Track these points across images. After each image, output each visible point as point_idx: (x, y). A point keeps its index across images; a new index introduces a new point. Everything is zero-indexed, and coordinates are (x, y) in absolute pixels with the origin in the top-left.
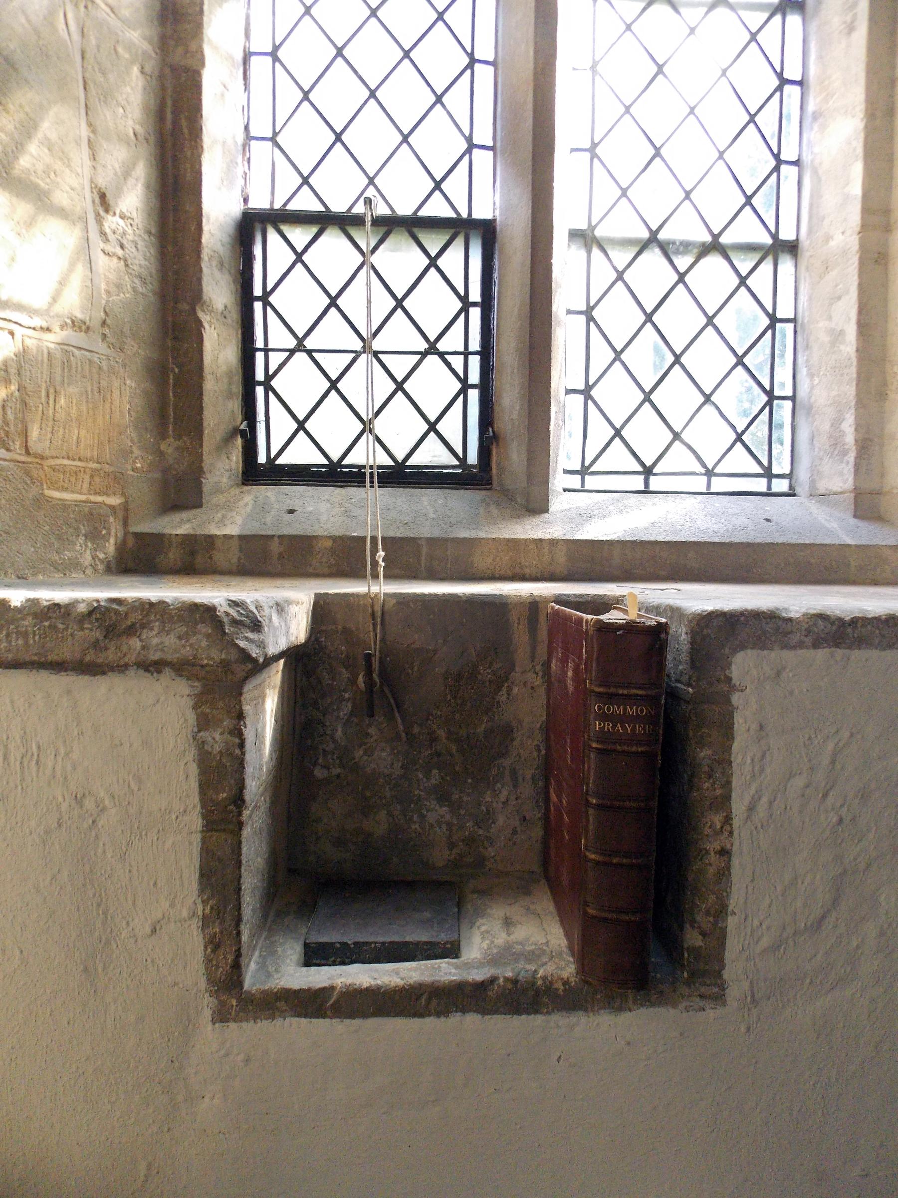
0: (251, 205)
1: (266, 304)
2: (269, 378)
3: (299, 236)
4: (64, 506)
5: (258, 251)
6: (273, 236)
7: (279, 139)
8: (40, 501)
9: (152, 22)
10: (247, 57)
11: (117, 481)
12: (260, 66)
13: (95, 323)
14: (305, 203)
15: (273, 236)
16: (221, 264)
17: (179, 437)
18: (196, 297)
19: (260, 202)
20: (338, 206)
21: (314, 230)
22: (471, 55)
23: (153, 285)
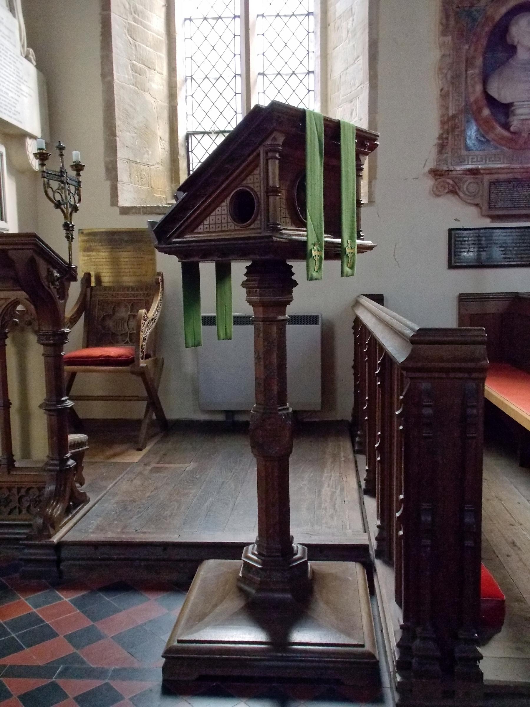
0: (188, 131)
1: (192, 152)
2: (192, 150)
3: (199, 137)
4: (157, 197)
5: (190, 141)
6: (193, 137)
7: (194, 115)
8: (154, 196)
9: (316, 601)
10: (186, 97)
11: (164, 192)
12: (189, 98)
13: (160, 162)
14: (200, 129)
15: (193, 137)
16: (182, 145)
17: (175, 183)
18: (178, 154)
19: (190, 130)
20: (207, 130)
21: (202, 135)
22: (235, 93)
23: (169, 153)
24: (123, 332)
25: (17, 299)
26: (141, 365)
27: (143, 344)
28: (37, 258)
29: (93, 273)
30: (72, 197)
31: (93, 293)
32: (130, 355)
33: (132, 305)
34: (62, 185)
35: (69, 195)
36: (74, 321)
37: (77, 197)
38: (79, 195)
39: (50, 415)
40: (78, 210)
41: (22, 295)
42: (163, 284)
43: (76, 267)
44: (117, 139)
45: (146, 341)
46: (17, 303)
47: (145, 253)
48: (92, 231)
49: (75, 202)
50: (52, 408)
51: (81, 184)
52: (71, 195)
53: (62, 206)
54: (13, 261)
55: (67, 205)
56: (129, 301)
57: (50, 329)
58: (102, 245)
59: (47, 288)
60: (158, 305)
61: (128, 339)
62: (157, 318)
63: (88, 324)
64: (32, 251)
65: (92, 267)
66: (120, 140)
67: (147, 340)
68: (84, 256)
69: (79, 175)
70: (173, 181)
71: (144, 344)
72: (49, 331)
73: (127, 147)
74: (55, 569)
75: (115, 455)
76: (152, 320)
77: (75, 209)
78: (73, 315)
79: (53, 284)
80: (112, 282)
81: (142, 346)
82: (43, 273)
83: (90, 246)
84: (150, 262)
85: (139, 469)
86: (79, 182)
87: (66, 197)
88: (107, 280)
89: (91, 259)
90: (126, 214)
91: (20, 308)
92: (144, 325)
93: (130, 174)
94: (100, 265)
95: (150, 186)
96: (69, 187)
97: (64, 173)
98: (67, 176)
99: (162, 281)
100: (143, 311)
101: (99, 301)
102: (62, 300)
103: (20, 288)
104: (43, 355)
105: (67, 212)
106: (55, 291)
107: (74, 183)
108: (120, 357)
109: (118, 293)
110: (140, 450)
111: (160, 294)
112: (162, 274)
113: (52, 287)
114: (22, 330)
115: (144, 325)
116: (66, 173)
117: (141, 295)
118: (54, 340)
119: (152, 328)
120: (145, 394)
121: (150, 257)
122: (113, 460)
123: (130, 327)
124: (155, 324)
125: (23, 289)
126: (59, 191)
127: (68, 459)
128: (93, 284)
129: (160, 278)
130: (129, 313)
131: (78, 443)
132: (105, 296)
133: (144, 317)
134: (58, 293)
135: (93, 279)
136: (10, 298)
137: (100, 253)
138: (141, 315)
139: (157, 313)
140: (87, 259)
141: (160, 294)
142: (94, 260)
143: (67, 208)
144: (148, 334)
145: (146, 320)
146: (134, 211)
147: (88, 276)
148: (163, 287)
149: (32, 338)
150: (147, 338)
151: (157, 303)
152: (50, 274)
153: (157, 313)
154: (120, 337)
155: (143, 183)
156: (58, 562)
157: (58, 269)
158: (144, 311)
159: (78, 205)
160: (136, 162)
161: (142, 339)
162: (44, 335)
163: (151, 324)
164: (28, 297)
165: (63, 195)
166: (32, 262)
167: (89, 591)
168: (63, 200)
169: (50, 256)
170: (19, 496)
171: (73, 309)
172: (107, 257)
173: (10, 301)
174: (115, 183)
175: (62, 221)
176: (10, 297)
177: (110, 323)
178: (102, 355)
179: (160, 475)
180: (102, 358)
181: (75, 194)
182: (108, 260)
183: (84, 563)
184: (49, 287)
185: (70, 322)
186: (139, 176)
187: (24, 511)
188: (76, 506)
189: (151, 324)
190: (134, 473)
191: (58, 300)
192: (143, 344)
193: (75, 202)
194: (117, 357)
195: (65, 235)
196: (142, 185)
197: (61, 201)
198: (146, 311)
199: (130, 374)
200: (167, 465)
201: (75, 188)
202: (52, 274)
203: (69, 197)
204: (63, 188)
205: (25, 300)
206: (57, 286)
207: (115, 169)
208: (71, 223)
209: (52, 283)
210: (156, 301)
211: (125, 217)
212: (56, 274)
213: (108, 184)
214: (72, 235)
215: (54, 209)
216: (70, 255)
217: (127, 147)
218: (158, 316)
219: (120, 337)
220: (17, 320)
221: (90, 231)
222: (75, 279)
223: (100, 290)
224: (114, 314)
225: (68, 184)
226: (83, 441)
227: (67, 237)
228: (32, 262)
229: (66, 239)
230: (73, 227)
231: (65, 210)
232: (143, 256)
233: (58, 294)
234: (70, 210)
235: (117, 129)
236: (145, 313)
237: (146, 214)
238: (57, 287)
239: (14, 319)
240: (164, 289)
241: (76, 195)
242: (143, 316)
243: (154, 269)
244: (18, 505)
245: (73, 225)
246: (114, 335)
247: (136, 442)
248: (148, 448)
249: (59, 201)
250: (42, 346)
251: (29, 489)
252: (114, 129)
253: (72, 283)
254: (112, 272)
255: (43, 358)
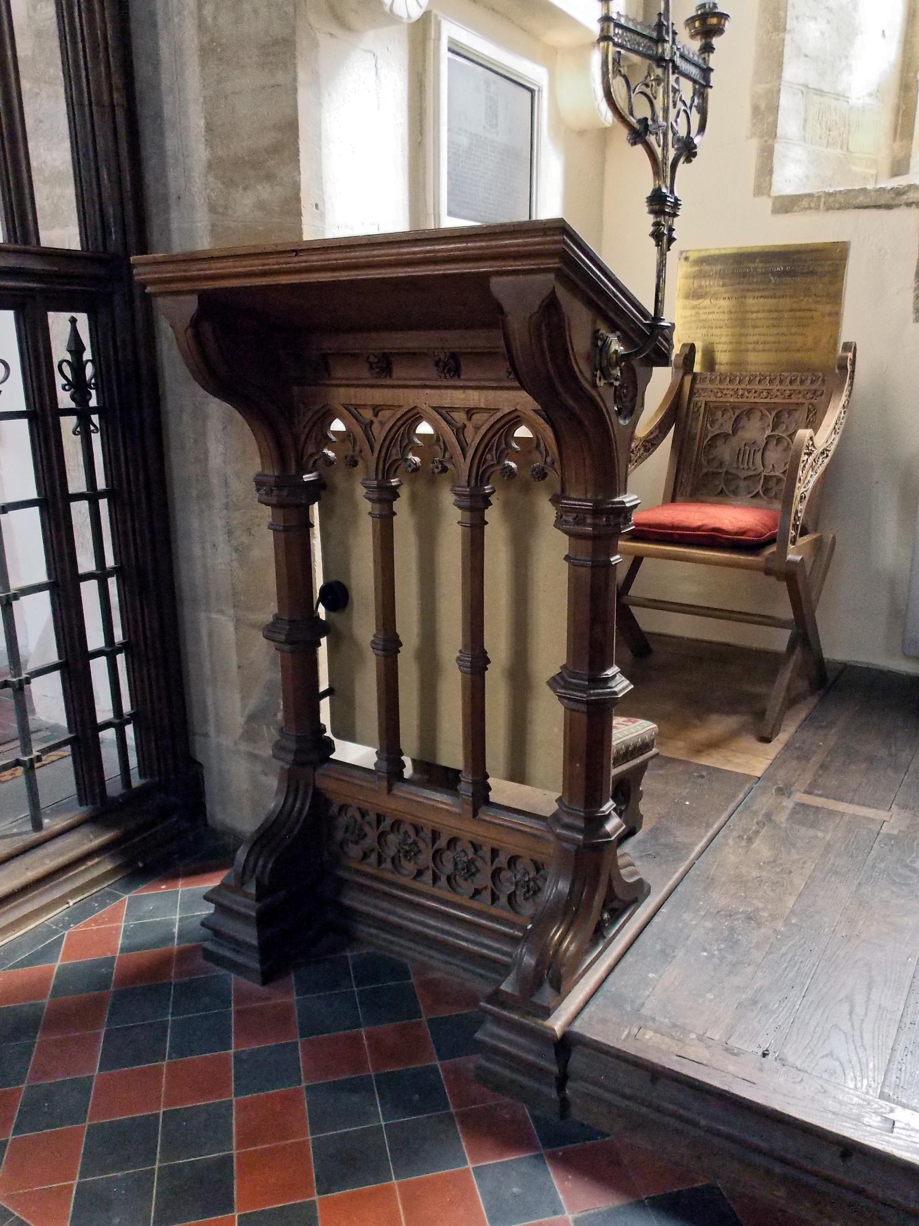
17: (901, 140)
24: (752, 473)
25: (516, 410)
26: (790, 557)
27: (800, 507)
28: (563, 295)
29: (699, 346)
30: (682, 114)
31: (697, 386)
32: (763, 530)
33: (778, 416)
34: (659, 71)
35: (675, 105)
36: (653, 445)
37: (695, 117)
38: (703, 112)
39: (572, 710)
40: (695, 155)
41: (523, 400)
42: (853, 371)
43: (673, 325)
44: (788, 37)
45: (805, 502)
46: (515, 420)
47: (819, 299)
48: (708, 253)
49: (689, 132)
50: (579, 695)
51: (713, 76)
52: (680, 105)
53: (652, 139)
54: (500, 309)
55: (665, 135)
56: (770, 407)
57: (589, 496)
58: (724, 285)
59: (587, 386)
60: (839, 418)
61: (759, 488)
62: (833, 448)
63: (679, 448)
64: (552, 276)
65: (699, 331)
66: (792, 40)
67: (807, 498)
68: (685, 308)
69: (708, 48)
70: (898, 136)
71: (800, 507)
72: (585, 501)
73: (806, 56)
74: (554, 1095)
75: (714, 745)
76: (823, 453)
77: (688, 150)
78: (651, 433)
79: (606, 375)
80: (727, 364)
81: (797, 512)
82: (580, 343)
83: (700, 287)
84: (827, 319)
85: (765, 801)
86: (707, 71)
87: (666, 111)
88: (722, 357)
89: (698, 313)
90: (786, 212)
91: (522, 432)
92: (804, 466)
93: (805, 120)
94: (716, 328)
95: (845, 148)
96: (677, 80)
97: (667, 33)
98: (674, 42)
99: (853, 363)
100: (804, 433)
101: (706, 404)
102: (625, 418)
103: (517, 384)
104: (567, 558)
105: (665, 157)
106: (609, 395)
107: (694, 72)
108: (743, 533)
109: (748, 387)
110: (766, 740)
111: (845, 393)
112: (855, 348)
113: (601, 383)
114: (526, 489)
115: (804, 466)
116: (675, 33)
117: (800, 393)
118: (594, 525)
119: (821, 470)
120: (786, 612)
121: (828, 308)
122: (705, 761)
123: (766, 463)
124: (827, 461)
125: (523, 387)
126: (648, 91)
127: (607, 818)
128: (697, 368)
129: (850, 355)
130: (768, 432)
131: (635, 747)
132: (720, 394)
133: (807, 447)
134: (617, 398)
135: (698, 357)
136: (498, 410)
137: (717, 302)
138: (802, 442)
139: (833, 436)
140: (691, 316)
141: (845, 393)
142: (703, 317)
143: (665, 147)
144: (811, 485)
145: (809, 454)
146: (805, 203)
147: (691, 349)
148: (852, 378)
149: (547, 511)
150: (807, 494)
151: (837, 413)
152: (599, 346)
153: (833, 436)
154: (742, 484)
155: (830, 140)
156: (562, 1080)
157: (624, 332)
158: (808, 432)
159: (697, 140)
160: (820, 92)
161: (799, 498)
162: (572, 510)
163: (820, 462)
164: (539, 407)
165: (659, 103)
166: (551, 305)
167: (631, 1200)
168: (654, 120)
169: (601, 292)
170: (493, 868)
171: (652, 420)
172: (733, 310)
173: (499, 415)
174: (770, 142)
175: (647, 185)
176: (501, 407)
177: (725, 452)
178: (703, 526)
179: (816, 837)
180: (704, 531)
181: (691, 108)
182: (733, 316)
183: (624, 1103)
184: (595, 386)
185: (644, 446)
186: (824, 125)
187: (503, 900)
188: (616, 915)
189: (820, 462)
190: (755, 813)
191: (613, 417)
192: (800, 507)
193: (689, 132)
194: (736, 534)
195: (651, 229)
196: (828, 145)
197: (650, 122)
198: (813, 434)
199: (762, 574)
200: (832, 804)
201: (695, 90)
202: (606, 345)
203: (672, 113)
204: (658, 80)
205: (532, 414)
206: (616, 380)
207: (774, 109)
208: (672, 192)
209: (602, 372)
210: (835, 407)
211: (783, 219)
212: (616, 347)
213: (754, 144)
214: (671, 230)
215: (629, 145)
216: (659, 289)
217: (806, 56)
218: (835, 443)
219: (742, 484)
220: (513, 465)
221: (703, 254)
222: (663, 359)
223: (711, 381)
224: (735, 431)
225: (676, 68)
226: (647, 740)
227: (657, 236)
228: (551, 305)
229: (653, 242)
230: (676, 204)
231: (659, 151)
232: (813, 306)
233: (615, 402)
234: (672, 153)
235: (788, 13)
236: (811, 439)
237: (832, 208)
238: (617, 383)
239: (506, 462)
240: (855, 381)
241: (694, 109)
242: (806, 444)
243: (835, 338)
244: (490, 884)
245: (676, 199)
246: (730, 477)
247: (760, 715)
248: (783, 737)
249: (646, 119)
250: (567, 537)
251: (513, 861)
252: (782, 14)
253: (656, 370)
254: (731, 343)
255: (566, 565)
